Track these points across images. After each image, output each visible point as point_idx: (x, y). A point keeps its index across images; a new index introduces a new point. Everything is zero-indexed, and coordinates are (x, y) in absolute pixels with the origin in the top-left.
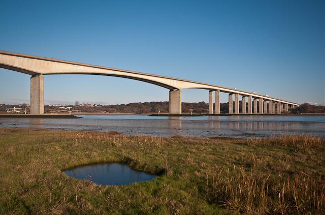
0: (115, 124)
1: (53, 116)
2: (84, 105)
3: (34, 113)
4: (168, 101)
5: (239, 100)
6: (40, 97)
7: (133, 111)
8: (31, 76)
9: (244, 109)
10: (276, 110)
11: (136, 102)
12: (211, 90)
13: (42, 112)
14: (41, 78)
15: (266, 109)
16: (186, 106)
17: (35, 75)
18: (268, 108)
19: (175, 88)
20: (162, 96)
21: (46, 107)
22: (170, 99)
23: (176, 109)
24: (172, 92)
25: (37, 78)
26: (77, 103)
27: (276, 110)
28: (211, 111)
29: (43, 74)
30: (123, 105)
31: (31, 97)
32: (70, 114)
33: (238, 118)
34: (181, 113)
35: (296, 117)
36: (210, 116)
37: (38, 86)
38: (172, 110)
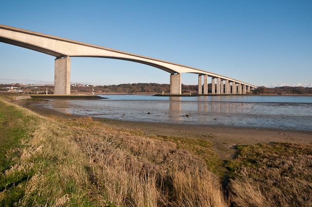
0: (282, 110)
3: (61, 93)
4: (169, 84)
5: (208, 83)
7: (125, 91)
8: (55, 58)
9: (213, 90)
10: (237, 91)
12: (200, 75)
13: (68, 93)
14: (68, 60)
15: (222, 90)
16: (185, 88)
17: (59, 56)
18: (237, 89)
19: (175, 72)
20: (163, 78)
21: (72, 88)
23: (176, 90)
27: (237, 91)
28: (200, 92)
29: (70, 56)
30: (114, 86)
32: (93, 95)
33: (208, 98)
34: (181, 93)
35: (309, 98)
36: (205, 97)
37: (64, 68)
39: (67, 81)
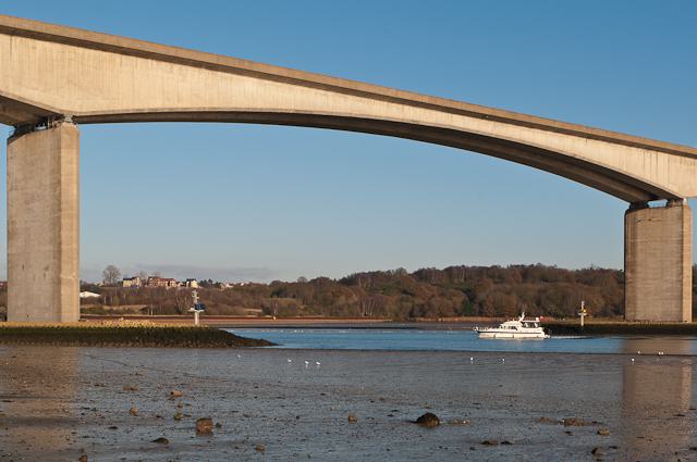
1: (139, 332)
2: (144, 283)
4: (620, 267)
6: (64, 234)
7: (379, 310)
11: (384, 269)
13: (71, 317)
20: (576, 234)
22: (629, 249)
24: (640, 214)
25: (43, 136)
26: (112, 272)
29: (79, 120)
30: (321, 283)
31: (11, 235)
34: (687, 317)
35: (420, 334)
37: (47, 181)
38: (640, 303)
39: (64, 247)
